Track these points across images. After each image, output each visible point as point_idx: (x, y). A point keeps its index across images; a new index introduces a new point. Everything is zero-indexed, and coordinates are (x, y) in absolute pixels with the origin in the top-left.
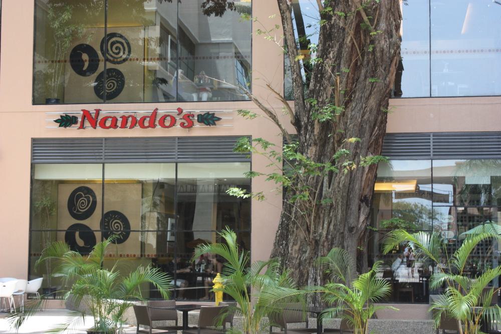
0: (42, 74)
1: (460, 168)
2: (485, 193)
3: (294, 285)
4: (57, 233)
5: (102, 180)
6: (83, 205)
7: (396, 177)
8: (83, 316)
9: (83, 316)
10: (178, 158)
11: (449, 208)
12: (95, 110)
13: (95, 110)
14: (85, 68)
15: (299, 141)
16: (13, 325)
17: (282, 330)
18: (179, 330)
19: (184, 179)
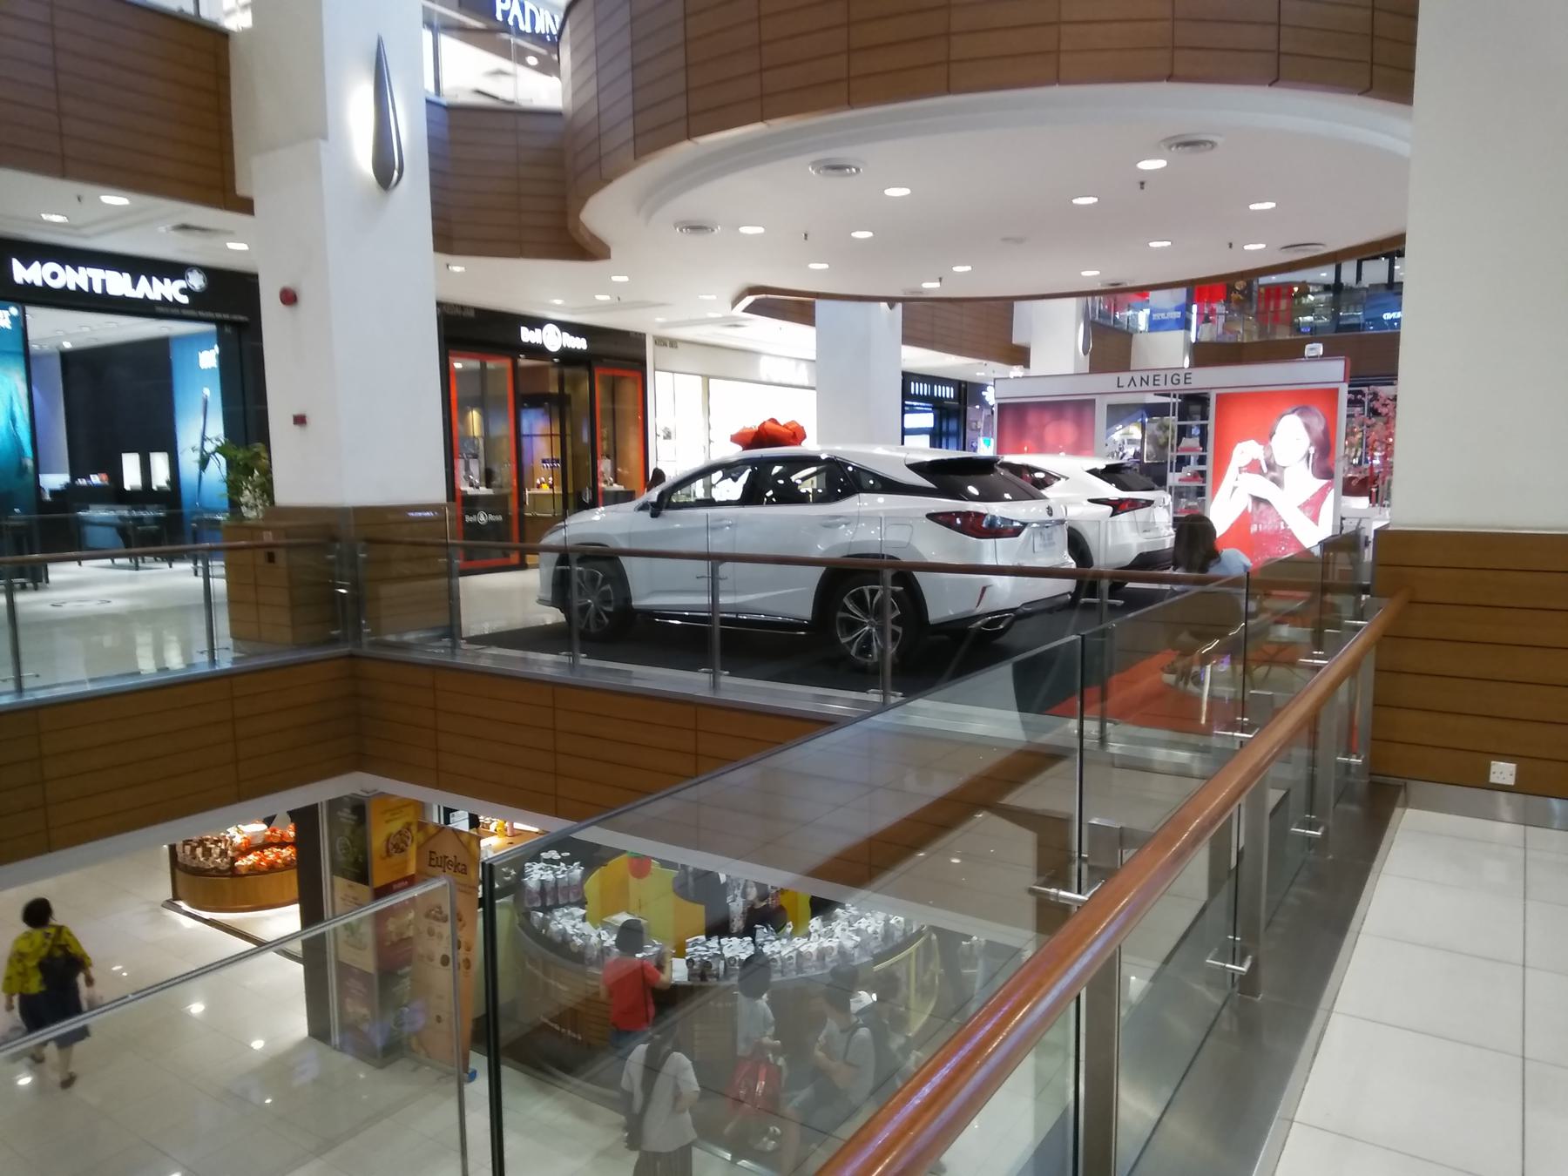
0: (1353, 770)
1: (524, 914)
2: (1367, 537)
3: (13, 520)
4: (1286, 54)
5: (1085, 721)
6: (1176, 377)
7: (1333, 530)
8: (909, 544)
9: (909, 544)
10: (439, 807)
11: (337, 913)
12: (77, 272)
13: (77, 272)
14: (499, 518)
15: (1315, 334)
16: (1029, 886)
17: (131, 561)
18: (485, 365)
19: (73, 695)
